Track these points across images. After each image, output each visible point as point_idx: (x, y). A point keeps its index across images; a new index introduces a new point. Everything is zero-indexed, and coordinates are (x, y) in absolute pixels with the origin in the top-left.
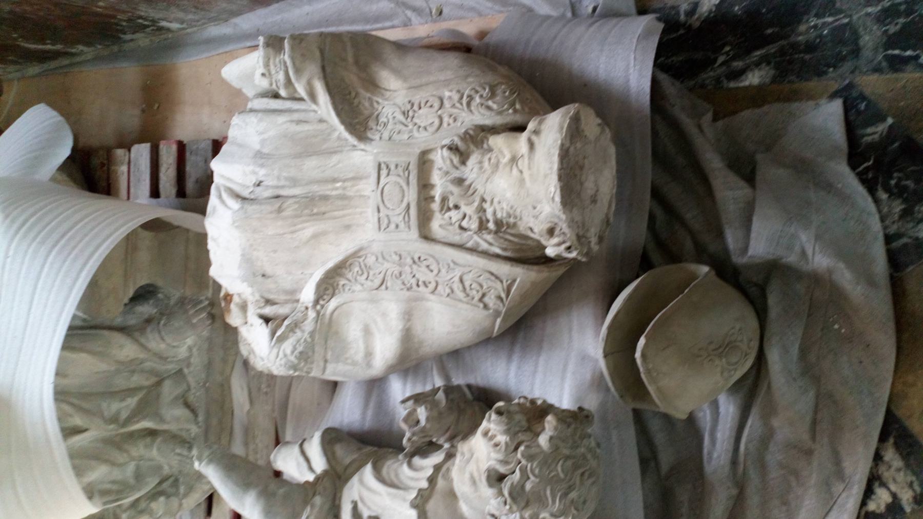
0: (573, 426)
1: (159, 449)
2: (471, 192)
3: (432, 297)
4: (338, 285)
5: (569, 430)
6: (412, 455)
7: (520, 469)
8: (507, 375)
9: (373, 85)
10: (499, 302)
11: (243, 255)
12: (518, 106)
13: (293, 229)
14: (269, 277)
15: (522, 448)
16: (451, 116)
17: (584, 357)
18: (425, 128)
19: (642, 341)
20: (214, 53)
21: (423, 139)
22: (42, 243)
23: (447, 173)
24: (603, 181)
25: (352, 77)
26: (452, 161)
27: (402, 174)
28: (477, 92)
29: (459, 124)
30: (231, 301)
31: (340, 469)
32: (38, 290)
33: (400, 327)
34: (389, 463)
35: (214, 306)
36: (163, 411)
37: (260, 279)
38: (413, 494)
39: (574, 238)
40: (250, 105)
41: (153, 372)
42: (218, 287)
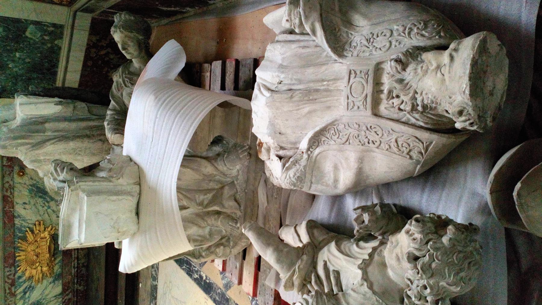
0: (465, 234)
1: (221, 221)
2: (408, 87)
3: (377, 150)
4: (321, 140)
5: (463, 236)
6: (359, 240)
7: (429, 255)
8: (421, 201)
9: (349, 24)
10: (420, 155)
11: (270, 122)
12: (442, 34)
13: (298, 108)
14: (283, 134)
15: (431, 243)
16: (397, 41)
17: (474, 194)
18: (380, 49)
19: (519, 185)
20: (256, 9)
21: (378, 56)
22: (173, 112)
23: (393, 76)
24: (499, 82)
25: (337, 20)
26: (396, 68)
27: (363, 77)
28: (415, 25)
29: (402, 46)
30: (262, 146)
31: (316, 243)
32: (170, 136)
33: (356, 167)
34: (345, 243)
35: (253, 150)
36: (224, 202)
37: (278, 135)
38: (360, 262)
39: (476, 117)
40: (277, 38)
41: (219, 182)
42: (255, 138)
